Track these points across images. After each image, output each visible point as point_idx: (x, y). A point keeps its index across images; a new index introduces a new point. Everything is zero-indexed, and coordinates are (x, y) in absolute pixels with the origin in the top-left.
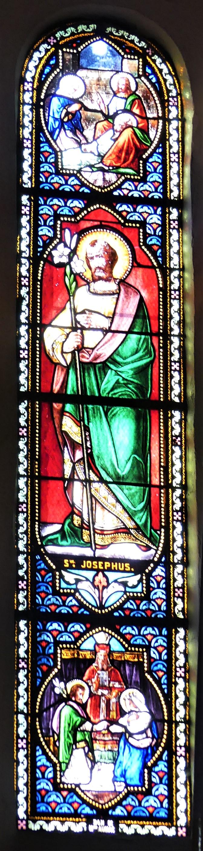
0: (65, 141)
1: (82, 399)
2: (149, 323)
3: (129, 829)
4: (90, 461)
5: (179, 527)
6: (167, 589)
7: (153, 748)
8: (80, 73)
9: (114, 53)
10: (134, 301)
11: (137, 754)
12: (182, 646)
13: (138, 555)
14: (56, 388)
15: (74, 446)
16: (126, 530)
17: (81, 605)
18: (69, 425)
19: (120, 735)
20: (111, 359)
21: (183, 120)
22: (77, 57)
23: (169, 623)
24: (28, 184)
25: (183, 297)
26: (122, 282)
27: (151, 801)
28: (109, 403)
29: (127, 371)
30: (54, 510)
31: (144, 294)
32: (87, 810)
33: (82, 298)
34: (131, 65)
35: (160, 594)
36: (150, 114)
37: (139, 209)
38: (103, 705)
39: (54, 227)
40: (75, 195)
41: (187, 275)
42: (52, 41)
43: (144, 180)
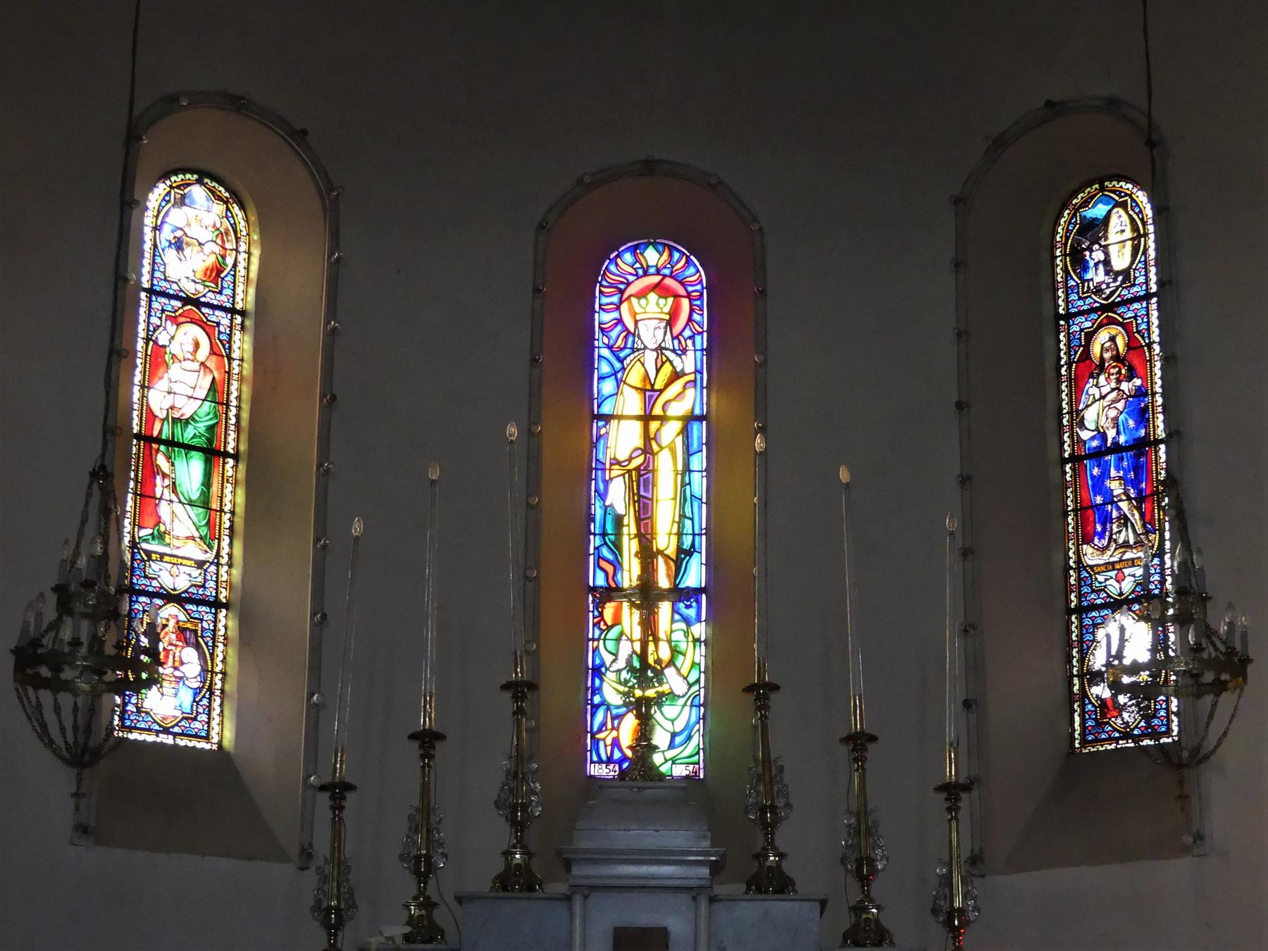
0: (170, 255)
1: (171, 443)
2: (217, 394)
3: (182, 742)
4: (174, 488)
5: (227, 540)
6: (217, 582)
7: (201, 689)
8: (184, 208)
9: (208, 199)
10: (209, 378)
11: (191, 692)
12: (223, 621)
13: (202, 557)
14: (155, 433)
15: (164, 476)
16: (193, 538)
17: (162, 587)
18: (161, 461)
19: (181, 678)
20: (192, 418)
21: (249, 253)
22: (183, 197)
23: (216, 604)
24: (146, 285)
25: (241, 379)
26: (202, 364)
27: (197, 725)
28: (189, 448)
29: (202, 427)
30: (150, 521)
31: (216, 374)
32: (157, 727)
33: (175, 371)
34: (219, 208)
35: (212, 584)
36: (228, 246)
37: (217, 313)
38: (171, 657)
39: (160, 318)
40: (176, 297)
41: (245, 365)
42: (168, 183)
43: (220, 293)
